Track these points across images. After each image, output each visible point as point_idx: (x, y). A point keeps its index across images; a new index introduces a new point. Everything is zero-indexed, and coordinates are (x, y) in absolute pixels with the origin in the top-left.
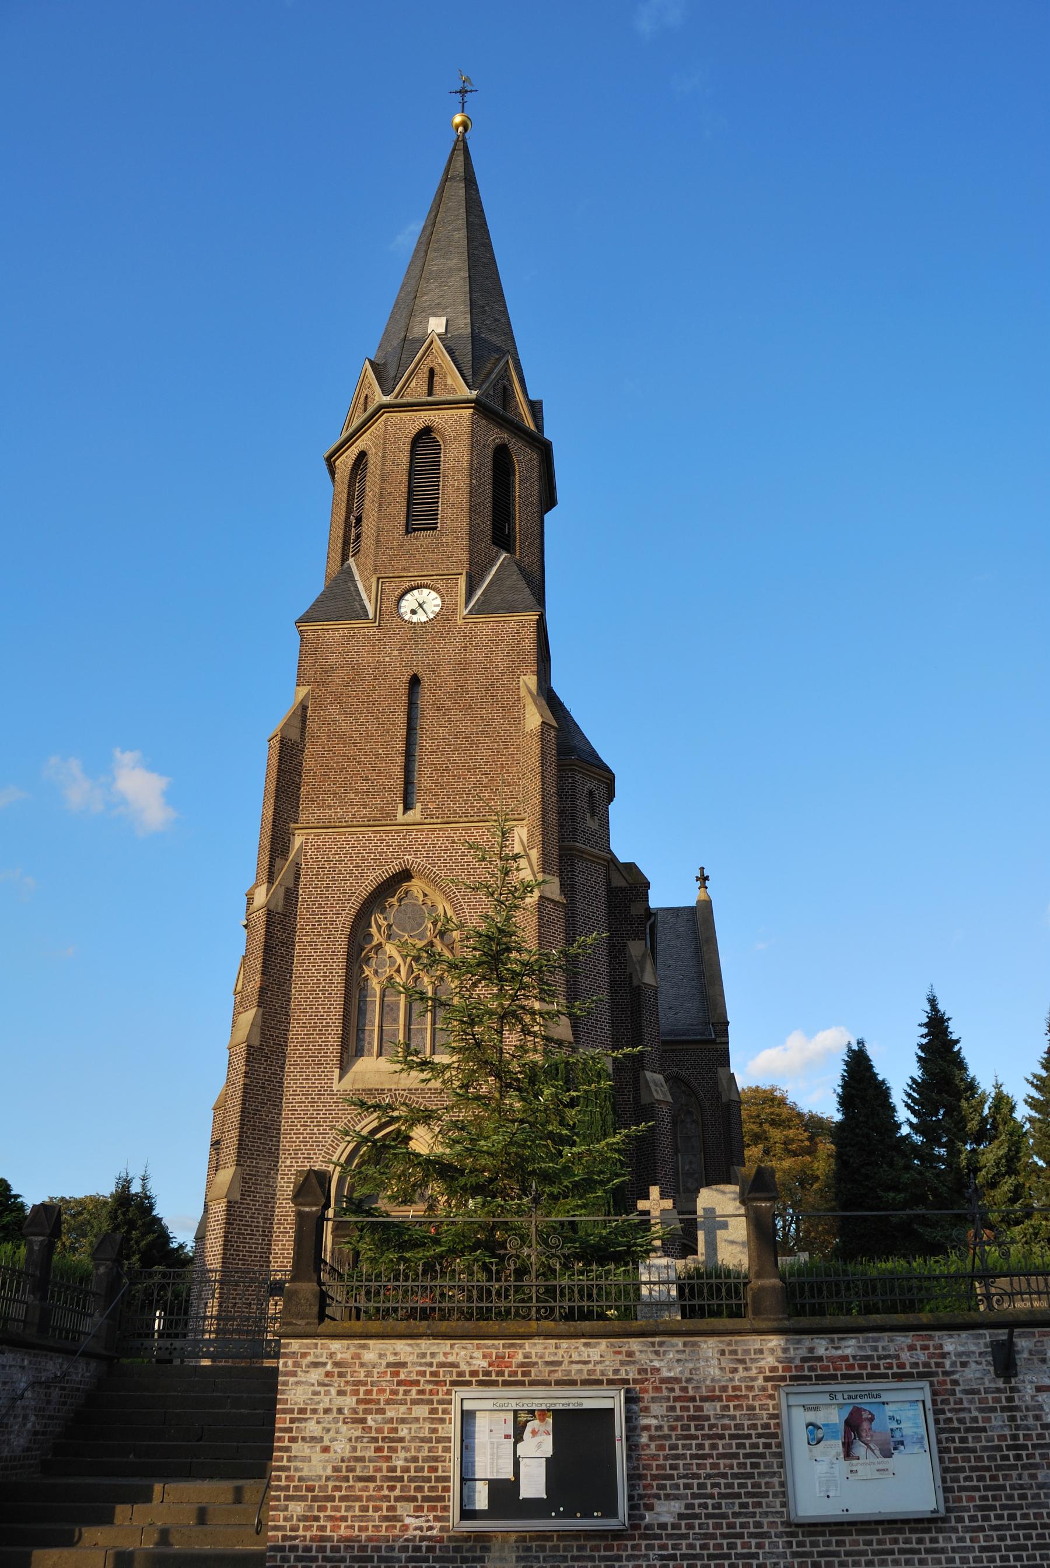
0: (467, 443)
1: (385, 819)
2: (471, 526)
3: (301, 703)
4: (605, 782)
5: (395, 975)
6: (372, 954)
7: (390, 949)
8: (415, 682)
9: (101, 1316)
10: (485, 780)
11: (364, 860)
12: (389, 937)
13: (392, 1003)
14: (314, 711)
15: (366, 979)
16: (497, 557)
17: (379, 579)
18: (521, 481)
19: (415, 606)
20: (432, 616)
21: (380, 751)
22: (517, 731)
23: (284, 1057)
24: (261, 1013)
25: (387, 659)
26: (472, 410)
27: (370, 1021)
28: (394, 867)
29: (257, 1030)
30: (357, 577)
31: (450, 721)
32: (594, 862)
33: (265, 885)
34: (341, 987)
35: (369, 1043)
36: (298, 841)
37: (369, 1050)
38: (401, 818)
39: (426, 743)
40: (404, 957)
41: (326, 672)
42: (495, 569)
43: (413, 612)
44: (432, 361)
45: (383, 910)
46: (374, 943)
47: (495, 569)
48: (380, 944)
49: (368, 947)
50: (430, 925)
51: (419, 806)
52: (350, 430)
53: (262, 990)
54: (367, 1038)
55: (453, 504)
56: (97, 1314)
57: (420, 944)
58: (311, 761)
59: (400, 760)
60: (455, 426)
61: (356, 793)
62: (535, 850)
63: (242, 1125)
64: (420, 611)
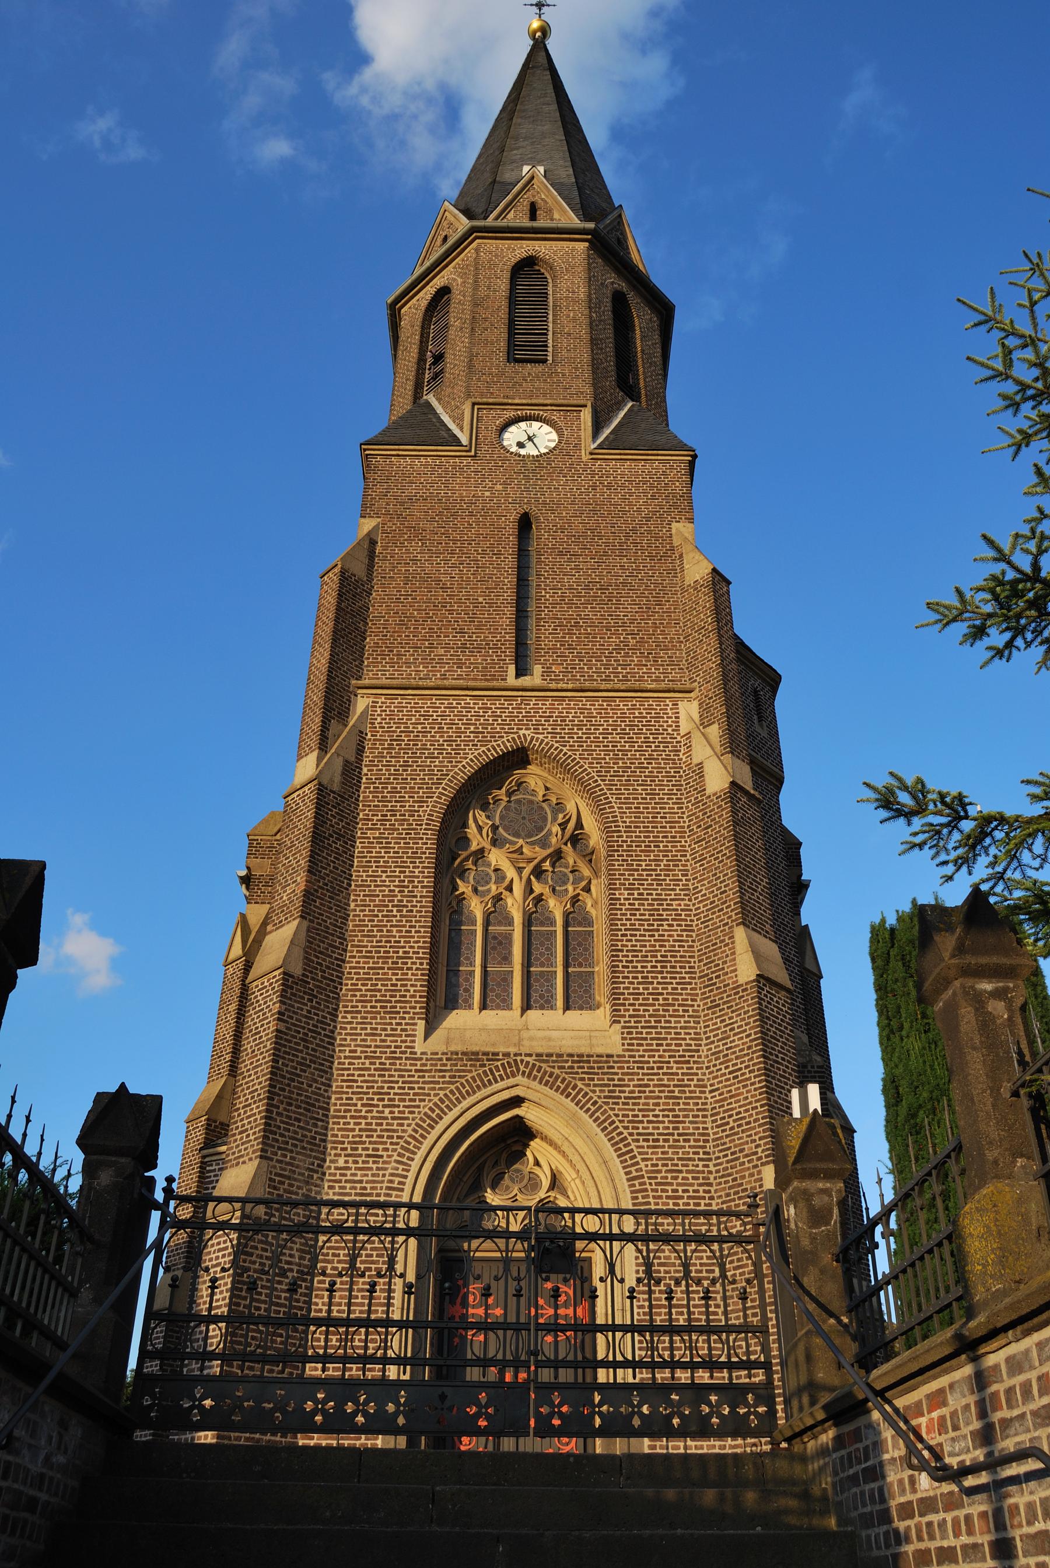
0: (583, 275)
1: (489, 686)
2: (593, 359)
3: (369, 534)
4: (772, 679)
5: (506, 893)
6: (469, 864)
7: (496, 857)
8: (525, 523)
9: (98, 1300)
10: (632, 642)
11: (459, 732)
12: (494, 842)
13: (500, 934)
14: (385, 548)
15: (461, 899)
16: (619, 406)
17: (474, 404)
18: (643, 337)
19: (523, 438)
20: (543, 451)
21: (481, 599)
22: (673, 585)
23: (338, 999)
24: (305, 929)
25: (487, 494)
26: (587, 244)
27: (467, 959)
28: (504, 744)
29: (298, 953)
30: (439, 409)
31: (578, 569)
32: (766, 779)
33: (315, 754)
34: (427, 903)
35: (466, 990)
36: (361, 704)
37: (466, 1001)
38: (511, 680)
39: (544, 593)
40: (520, 870)
41: (402, 504)
42: (622, 414)
43: (521, 445)
44: (534, 196)
45: (485, 807)
46: (474, 847)
47: (622, 414)
48: (482, 851)
49: (464, 854)
50: (556, 829)
51: (538, 669)
52: (427, 264)
53: (309, 896)
54: (464, 985)
55: (569, 334)
56: (86, 1294)
57: (541, 853)
58: (380, 605)
59: (509, 612)
60: (568, 262)
61: (447, 647)
62: (716, 726)
63: (271, 1095)
64: (529, 445)
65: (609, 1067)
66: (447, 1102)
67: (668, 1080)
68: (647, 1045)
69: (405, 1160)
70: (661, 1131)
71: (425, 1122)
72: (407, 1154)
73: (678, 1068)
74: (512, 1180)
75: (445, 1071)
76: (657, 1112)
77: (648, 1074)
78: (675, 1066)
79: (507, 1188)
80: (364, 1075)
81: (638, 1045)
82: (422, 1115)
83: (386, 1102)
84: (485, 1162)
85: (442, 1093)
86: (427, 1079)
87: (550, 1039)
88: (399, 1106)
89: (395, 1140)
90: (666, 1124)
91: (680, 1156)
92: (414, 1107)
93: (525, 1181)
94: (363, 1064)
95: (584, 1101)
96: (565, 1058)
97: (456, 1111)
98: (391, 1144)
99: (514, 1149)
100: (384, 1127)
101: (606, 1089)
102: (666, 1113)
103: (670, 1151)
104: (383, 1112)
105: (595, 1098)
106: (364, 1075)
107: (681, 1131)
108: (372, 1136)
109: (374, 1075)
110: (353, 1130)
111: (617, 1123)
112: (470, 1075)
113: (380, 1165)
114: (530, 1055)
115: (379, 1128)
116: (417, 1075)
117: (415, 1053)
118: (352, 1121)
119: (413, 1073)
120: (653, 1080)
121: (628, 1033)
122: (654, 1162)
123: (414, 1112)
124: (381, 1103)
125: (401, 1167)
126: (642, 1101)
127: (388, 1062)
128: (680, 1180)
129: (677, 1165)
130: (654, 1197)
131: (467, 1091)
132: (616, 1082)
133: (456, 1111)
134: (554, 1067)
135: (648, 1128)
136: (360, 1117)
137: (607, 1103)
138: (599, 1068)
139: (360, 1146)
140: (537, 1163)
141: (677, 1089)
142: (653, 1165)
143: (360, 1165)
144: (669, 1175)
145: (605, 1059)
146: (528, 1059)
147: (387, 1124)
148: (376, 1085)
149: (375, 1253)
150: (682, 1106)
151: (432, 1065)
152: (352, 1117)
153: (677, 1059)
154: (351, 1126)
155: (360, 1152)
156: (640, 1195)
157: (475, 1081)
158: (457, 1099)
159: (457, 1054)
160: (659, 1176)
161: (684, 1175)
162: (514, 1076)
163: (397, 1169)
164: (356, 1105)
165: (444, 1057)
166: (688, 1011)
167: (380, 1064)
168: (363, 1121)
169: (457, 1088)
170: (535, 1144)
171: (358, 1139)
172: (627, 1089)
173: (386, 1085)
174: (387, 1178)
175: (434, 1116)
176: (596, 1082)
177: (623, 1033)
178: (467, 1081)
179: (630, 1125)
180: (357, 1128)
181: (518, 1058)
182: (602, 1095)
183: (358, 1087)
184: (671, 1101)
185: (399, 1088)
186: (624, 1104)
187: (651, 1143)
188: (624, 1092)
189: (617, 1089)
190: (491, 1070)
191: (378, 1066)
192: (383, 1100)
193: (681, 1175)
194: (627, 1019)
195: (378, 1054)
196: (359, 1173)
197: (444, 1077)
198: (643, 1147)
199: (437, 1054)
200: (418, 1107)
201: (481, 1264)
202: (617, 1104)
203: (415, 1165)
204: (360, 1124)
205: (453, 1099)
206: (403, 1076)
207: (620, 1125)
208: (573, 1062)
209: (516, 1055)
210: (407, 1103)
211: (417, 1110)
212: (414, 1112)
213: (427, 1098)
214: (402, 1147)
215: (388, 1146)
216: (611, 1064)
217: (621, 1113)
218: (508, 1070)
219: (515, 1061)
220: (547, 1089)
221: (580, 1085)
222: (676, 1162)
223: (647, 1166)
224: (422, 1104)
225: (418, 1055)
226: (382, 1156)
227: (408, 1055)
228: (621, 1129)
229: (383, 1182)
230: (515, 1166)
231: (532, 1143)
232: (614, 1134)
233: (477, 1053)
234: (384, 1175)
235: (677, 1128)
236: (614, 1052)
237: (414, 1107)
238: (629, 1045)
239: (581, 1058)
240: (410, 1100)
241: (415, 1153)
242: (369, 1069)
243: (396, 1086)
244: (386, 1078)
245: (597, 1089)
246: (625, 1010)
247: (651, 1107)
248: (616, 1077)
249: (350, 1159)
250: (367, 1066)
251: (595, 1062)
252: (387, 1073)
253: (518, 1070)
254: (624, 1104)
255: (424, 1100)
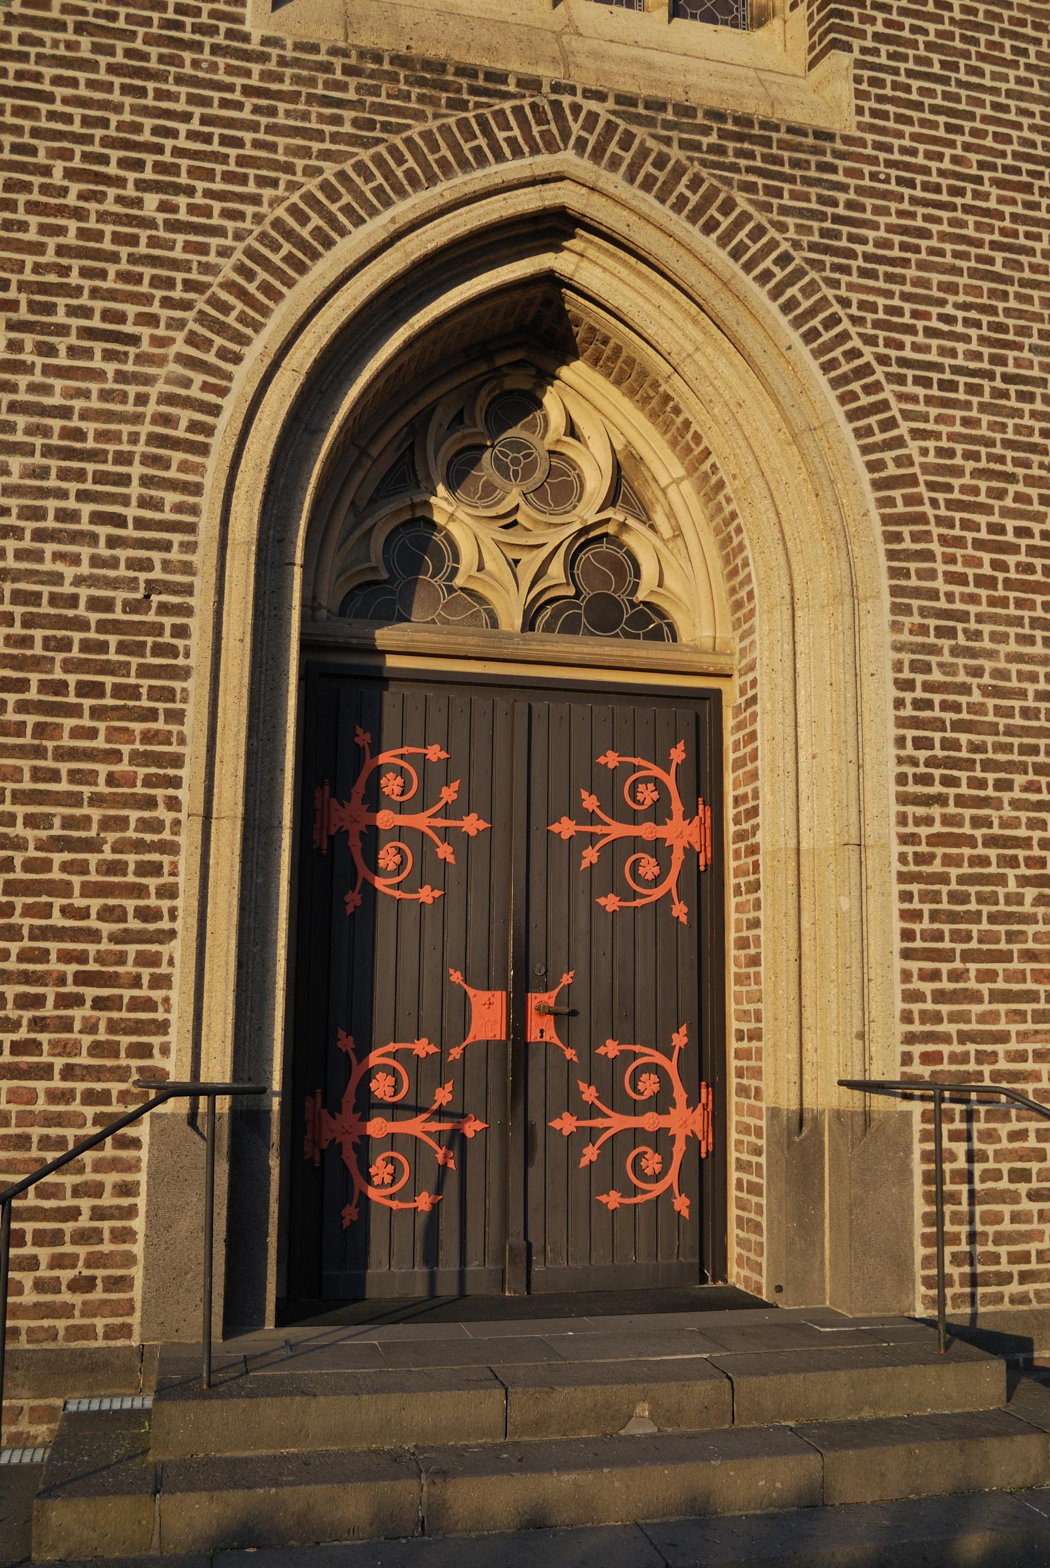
65: (822, 167)
66: (347, 198)
67: (978, 226)
68: (923, 123)
69: (211, 358)
70: (960, 361)
71: (276, 248)
72: (219, 341)
73: (1001, 200)
74: (502, 469)
75: (340, 103)
76: (949, 310)
77: (926, 203)
78: (995, 192)
79: (489, 489)
80: (74, 83)
81: (900, 119)
82: (266, 226)
83: (148, 174)
84: (431, 409)
85: (330, 169)
86: (281, 120)
87: (650, 66)
88: (190, 191)
89: (177, 294)
90: (974, 346)
91: (1010, 435)
92: (242, 198)
93: (539, 475)
94: (70, 46)
95: (754, 248)
96: (700, 120)
97: (376, 228)
98: (167, 302)
99: (509, 384)
100: (143, 249)
101: (816, 225)
102: (973, 314)
103: (985, 418)
104: (138, 203)
105: (785, 246)
106: (74, 83)
107: (1011, 369)
108: (103, 274)
109: (109, 87)
110: (39, 248)
111: (846, 324)
112: (417, 129)
113: (129, 367)
114: (600, 96)
115: (124, 251)
116: (249, 102)
117: (246, 38)
118: (34, 220)
119: (237, 96)
120: (938, 220)
121: (874, 82)
122: (944, 443)
123: (240, 216)
124: (131, 176)
125: (199, 378)
126: (911, 273)
127: (154, 51)
128: (1008, 502)
129: (1002, 459)
130: (943, 540)
131: (410, 174)
132: (841, 211)
133: (376, 228)
134: (667, 141)
135: (927, 349)
136: (61, 211)
137: (818, 266)
138: (795, 164)
139: (61, 302)
140: (572, 430)
141: (999, 256)
142: (941, 452)
143: (62, 360)
144: (983, 485)
145: (810, 141)
146: (593, 105)
147: (153, 242)
148: (114, 119)
149: (113, 640)
150: (1012, 304)
151: (297, 79)
152: (33, 207)
153: (1000, 175)
154: (32, 235)
155: (60, 317)
156: (906, 530)
157: (435, 148)
158: (378, 191)
159: (378, 58)
160: (957, 483)
161: (1020, 488)
162: (552, 147)
163: (187, 383)
164: (47, 171)
165: (338, 62)
166: (1025, 53)
167: (129, 53)
168: (73, 225)
169: (378, 160)
170: (576, 373)
171: (52, 278)
172: (871, 234)
173: (148, 123)
174: (152, 408)
175: (305, 233)
176: (787, 202)
177: (858, 80)
178: (409, 142)
179: (882, 334)
180: (52, 242)
181: (566, 100)
182: (805, 239)
183: (52, 116)
184: (986, 285)
185: (192, 135)
186: (863, 273)
187: (935, 392)
188: (864, 241)
189: (845, 229)
190: (482, 121)
191: (119, 58)
192: (139, 165)
193: (1012, 488)
194: (869, 43)
195: (121, 24)
196: (58, 384)
197: (337, 120)
198: (914, 399)
199: (314, 48)
200: (256, 200)
201: (407, 690)
202: (846, 270)
203: (244, 378)
204: (62, 231)
205: (366, 189)
206: (206, 102)
207: (853, 330)
208: (723, 134)
209: (556, 88)
210: (218, 186)
211: (249, 210)
212: (240, 216)
213: (284, 178)
214: (203, 318)
215: (155, 308)
216: (829, 159)
217: (855, 297)
218: (535, 130)
219: (556, 105)
220: (650, 198)
221: (742, 202)
222: (998, 450)
223: (924, 452)
224: (267, 193)
225: (254, 45)
226: (134, 340)
227: (220, 40)
228: (856, 343)
229: (138, 419)
230: (511, 433)
231: (564, 372)
232: (837, 353)
233: (440, 67)
234: (142, 399)
235: (1002, 361)
236: (836, 126)
237: (242, 198)
238: (874, 113)
239: (745, 128)
240: (229, 177)
241: (244, 340)
242: (91, 66)
243: (182, 128)
244: (150, 101)
245: (791, 221)
246: (863, 19)
247: (935, 293)
248: (841, 197)
249: (29, 339)
250: (85, 53)
251: (783, 145)
252: (150, 86)
253: (565, 134)
254: (863, 273)
255: (274, 183)
